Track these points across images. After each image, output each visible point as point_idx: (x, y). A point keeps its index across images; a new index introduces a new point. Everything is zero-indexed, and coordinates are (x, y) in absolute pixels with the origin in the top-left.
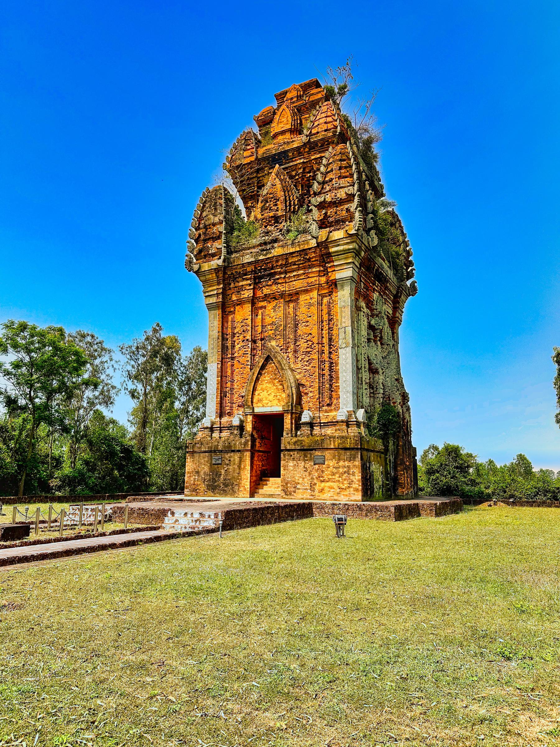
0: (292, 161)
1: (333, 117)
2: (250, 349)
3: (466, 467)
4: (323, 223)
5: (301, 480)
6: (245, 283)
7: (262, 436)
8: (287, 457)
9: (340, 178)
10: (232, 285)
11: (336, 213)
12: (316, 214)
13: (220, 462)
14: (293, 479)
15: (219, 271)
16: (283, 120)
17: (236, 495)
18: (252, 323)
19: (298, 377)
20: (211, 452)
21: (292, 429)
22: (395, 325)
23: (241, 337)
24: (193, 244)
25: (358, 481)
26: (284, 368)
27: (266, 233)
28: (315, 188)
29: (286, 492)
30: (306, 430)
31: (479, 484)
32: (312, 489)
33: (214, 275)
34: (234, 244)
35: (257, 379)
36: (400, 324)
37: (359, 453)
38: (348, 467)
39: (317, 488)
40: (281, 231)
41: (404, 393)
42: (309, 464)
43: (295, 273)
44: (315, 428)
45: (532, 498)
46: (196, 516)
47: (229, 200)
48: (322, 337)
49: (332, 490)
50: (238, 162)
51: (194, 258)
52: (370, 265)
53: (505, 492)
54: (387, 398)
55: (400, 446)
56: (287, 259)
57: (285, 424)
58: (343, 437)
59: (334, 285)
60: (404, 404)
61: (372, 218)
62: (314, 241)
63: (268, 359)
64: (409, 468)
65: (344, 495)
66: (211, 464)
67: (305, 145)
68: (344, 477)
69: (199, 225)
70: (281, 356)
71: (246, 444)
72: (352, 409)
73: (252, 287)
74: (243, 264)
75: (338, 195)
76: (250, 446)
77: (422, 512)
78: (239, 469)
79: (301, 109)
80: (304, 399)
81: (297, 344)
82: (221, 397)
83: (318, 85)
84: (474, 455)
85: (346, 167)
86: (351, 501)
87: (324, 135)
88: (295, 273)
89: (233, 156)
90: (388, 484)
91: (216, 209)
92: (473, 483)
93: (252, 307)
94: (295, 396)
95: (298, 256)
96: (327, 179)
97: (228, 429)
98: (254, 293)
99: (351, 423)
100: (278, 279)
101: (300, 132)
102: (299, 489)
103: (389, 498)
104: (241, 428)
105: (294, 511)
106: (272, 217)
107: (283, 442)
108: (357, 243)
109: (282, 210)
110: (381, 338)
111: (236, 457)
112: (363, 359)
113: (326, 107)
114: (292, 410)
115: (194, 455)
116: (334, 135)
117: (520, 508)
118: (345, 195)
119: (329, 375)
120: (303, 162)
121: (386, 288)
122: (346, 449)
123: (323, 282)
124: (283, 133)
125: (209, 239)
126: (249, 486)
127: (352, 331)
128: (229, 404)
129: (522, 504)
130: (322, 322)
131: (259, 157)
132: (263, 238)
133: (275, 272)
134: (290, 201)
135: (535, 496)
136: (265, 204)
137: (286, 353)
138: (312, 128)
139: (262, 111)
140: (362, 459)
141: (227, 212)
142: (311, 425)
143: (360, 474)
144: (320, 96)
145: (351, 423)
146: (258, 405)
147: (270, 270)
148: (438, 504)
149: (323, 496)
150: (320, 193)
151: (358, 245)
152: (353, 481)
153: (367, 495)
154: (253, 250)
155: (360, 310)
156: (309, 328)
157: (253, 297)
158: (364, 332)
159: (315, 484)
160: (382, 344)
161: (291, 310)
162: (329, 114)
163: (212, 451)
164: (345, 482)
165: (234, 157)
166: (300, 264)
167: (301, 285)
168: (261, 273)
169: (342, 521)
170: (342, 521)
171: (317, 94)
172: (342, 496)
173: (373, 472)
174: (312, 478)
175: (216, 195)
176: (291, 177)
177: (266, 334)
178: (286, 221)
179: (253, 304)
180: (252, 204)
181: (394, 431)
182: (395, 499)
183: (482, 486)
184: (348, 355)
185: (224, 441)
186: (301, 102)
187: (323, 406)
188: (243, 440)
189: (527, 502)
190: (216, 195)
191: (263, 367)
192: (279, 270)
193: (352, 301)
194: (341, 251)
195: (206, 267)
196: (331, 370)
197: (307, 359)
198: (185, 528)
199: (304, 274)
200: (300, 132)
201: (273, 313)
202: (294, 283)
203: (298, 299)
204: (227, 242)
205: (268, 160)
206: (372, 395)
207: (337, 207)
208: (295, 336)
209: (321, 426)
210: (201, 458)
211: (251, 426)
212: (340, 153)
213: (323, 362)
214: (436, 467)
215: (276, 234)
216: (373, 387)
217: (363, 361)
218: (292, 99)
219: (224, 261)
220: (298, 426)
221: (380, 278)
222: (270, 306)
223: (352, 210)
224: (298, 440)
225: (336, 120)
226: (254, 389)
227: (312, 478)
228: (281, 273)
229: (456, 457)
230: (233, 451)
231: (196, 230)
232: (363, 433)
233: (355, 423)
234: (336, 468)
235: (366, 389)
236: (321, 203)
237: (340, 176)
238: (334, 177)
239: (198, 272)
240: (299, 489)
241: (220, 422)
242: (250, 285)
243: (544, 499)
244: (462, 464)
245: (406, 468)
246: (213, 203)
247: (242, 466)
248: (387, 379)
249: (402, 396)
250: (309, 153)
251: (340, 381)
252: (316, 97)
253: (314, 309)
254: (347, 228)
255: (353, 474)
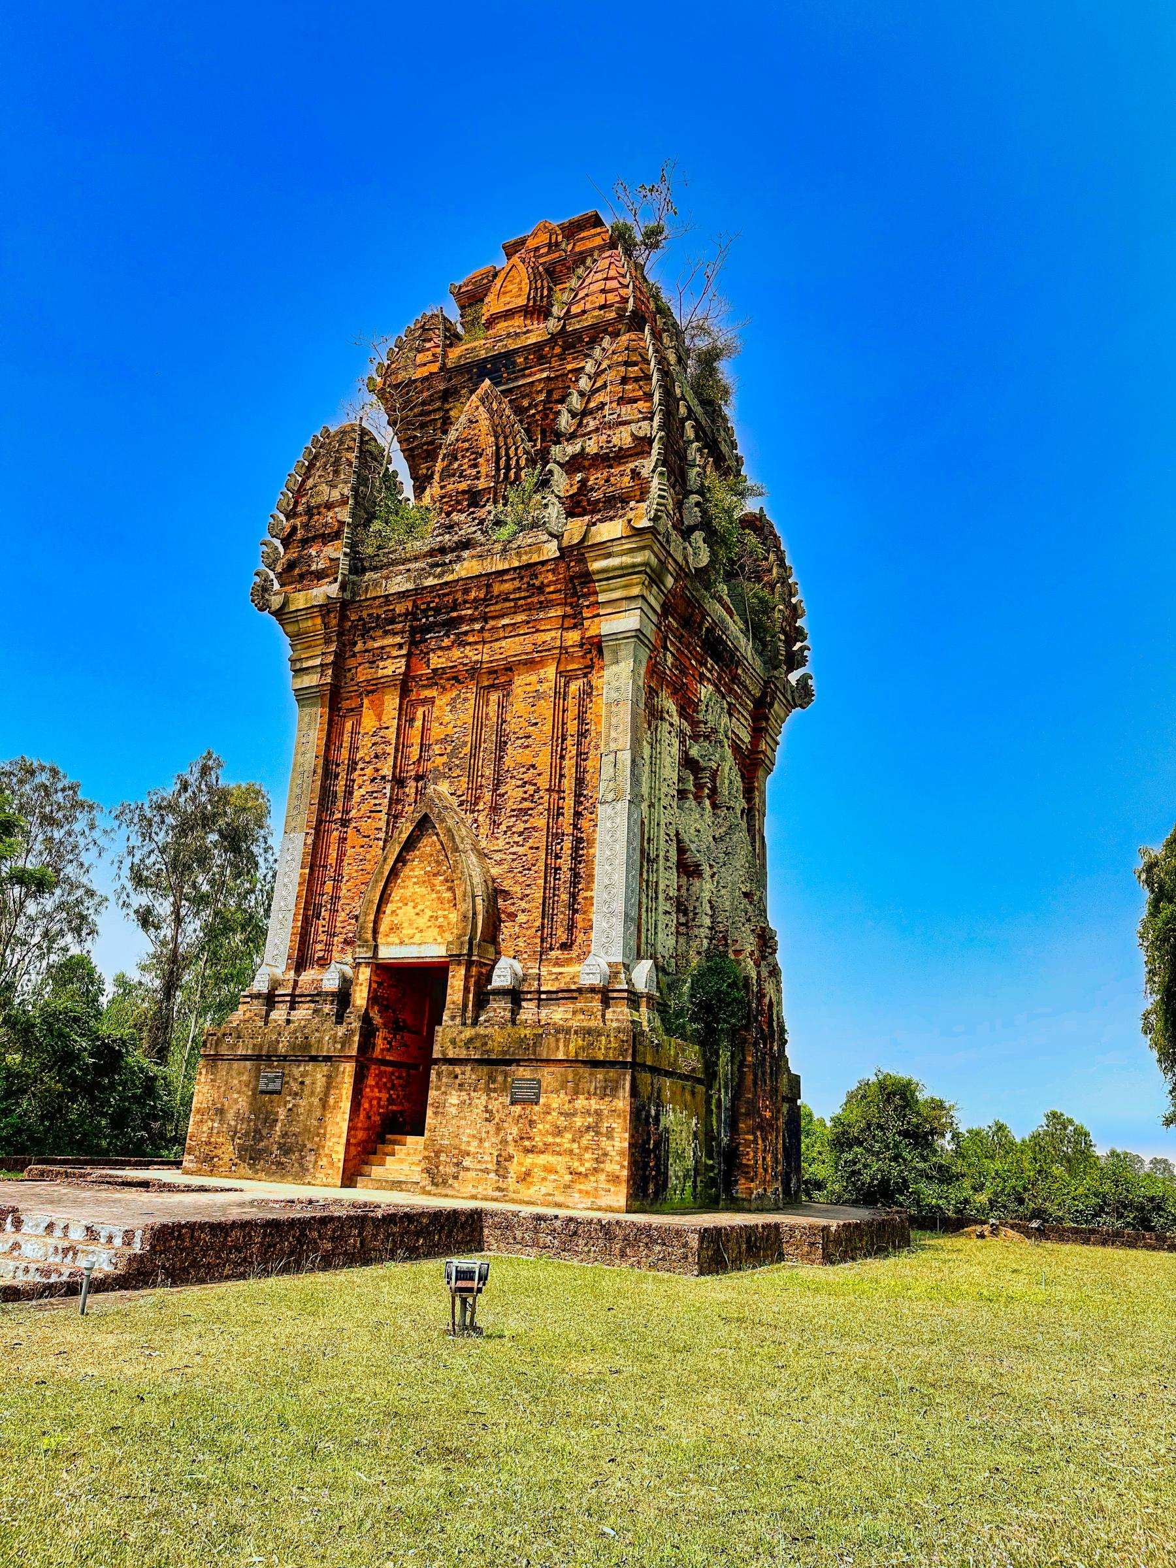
0: (524, 376)
1: (621, 279)
2: (386, 800)
3: (927, 1133)
4: (578, 504)
5: (475, 1143)
6: (390, 640)
7: (396, 1022)
8: (444, 1080)
9: (621, 401)
10: (359, 647)
11: (607, 481)
12: (562, 483)
13: (276, 1086)
14: (457, 1141)
15: (329, 612)
16: (509, 288)
17: (309, 1179)
18: (398, 737)
19: (494, 871)
20: (258, 1058)
21: (465, 1005)
22: (756, 770)
23: (369, 771)
24: (276, 548)
25: (621, 1153)
26: (461, 847)
27: (447, 528)
28: (563, 423)
29: (436, 1179)
30: (499, 1009)
31: (958, 1179)
32: (501, 1172)
33: (319, 621)
34: (370, 551)
35: (394, 873)
36: (769, 771)
37: (628, 1078)
38: (598, 1113)
39: (514, 1168)
40: (481, 522)
41: (763, 929)
42: (500, 1101)
43: (506, 621)
44: (524, 1004)
45: (1086, 1222)
46: (77, 1235)
47: (369, 454)
48: (562, 776)
49: (553, 1177)
50: (402, 376)
51: (275, 582)
52: (692, 615)
53: (1021, 1201)
54: (720, 939)
55: (747, 1066)
56: (489, 586)
57: (449, 991)
58: (589, 1032)
59: (595, 648)
60: (764, 958)
61: (698, 504)
62: (554, 544)
63: (424, 825)
64: (771, 1125)
65: (580, 1191)
66: (254, 1090)
67: (553, 338)
68: (584, 1142)
69: (295, 506)
70: (458, 822)
71: (346, 1040)
72: (620, 959)
73: (404, 652)
74: (387, 596)
75: (615, 440)
76: (356, 1046)
77: (788, 1249)
78: (324, 1108)
79: (554, 271)
80: (507, 929)
81: (501, 791)
82: (305, 916)
83: (597, 222)
84: (947, 1105)
85: (636, 380)
86: (599, 1209)
87: (596, 317)
88: (506, 621)
89: (393, 363)
90: (712, 1166)
91: (336, 472)
92: (945, 1175)
93: (402, 698)
94: (480, 919)
95: (514, 579)
96: (592, 405)
97: (313, 1002)
98: (408, 666)
99: (615, 995)
100: (466, 633)
101: (546, 314)
102: (468, 1169)
103: (710, 1205)
104: (343, 997)
105: (418, 1234)
106: (464, 492)
107: (438, 1038)
108: (653, 552)
109: (487, 476)
110: (714, 791)
111: (319, 1076)
112: (663, 837)
113: (607, 261)
114: (470, 954)
115: (216, 1066)
116: (620, 317)
117: (1056, 1246)
118: (630, 439)
119: (571, 869)
120: (548, 378)
121: (735, 678)
122: (595, 1064)
123: (570, 643)
124: (508, 314)
125: (315, 537)
126: (342, 1156)
127: (633, 761)
128: (323, 937)
129: (1062, 1236)
130: (564, 740)
131: (450, 365)
132: (438, 539)
133: (460, 617)
134: (509, 459)
135: (1095, 1216)
136: (451, 464)
137: (473, 812)
138: (571, 304)
139: (471, 275)
140: (634, 1092)
141: (362, 480)
142: (515, 996)
143: (627, 1135)
144: (598, 241)
145: (615, 995)
146: (389, 939)
147: (447, 613)
148: (833, 1229)
149: (530, 1192)
150: (572, 437)
151: (656, 556)
152: (606, 1155)
153: (646, 1195)
154: (412, 566)
155: (662, 719)
156: (531, 754)
157: (404, 674)
158: (670, 771)
159: (510, 1158)
160: (714, 806)
161: (492, 709)
162: (612, 273)
163: (263, 1058)
164: (587, 1156)
165: (393, 366)
166: (520, 599)
167: (519, 649)
168: (427, 617)
169: (472, 1279)
170: (472, 1279)
171: (592, 239)
172: (577, 1195)
173: (667, 1130)
174: (504, 1142)
175: (341, 443)
176: (519, 411)
177: (430, 765)
178: (495, 502)
179: (405, 692)
180: (428, 469)
181: (734, 1025)
182: (727, 1209)
183: (967, 1183)
184: (618, 820)
185: (295, 1031)
186: (557, 255)
187: (551, 949)
188: (341, 1031)
189: (1076, 1231)
190: (341, 443)
191: (410, 844)
192: (470, 612)
193: (636, 689)
194: (615, 569)
195: (300, 601)
196: (576, 857)
197: (520, 827)
198: (26, 1270)
199: (528, 622)
200: (546, 314)
201: (450, 715)
202: (503, 643)
203: (510, 682)
204: (353, 545)
205: (469, 371)
206: (683, 929)
207: (611, 467)
208: (497, 772)
209: (540, 1000)
210: (234, 1073)
211: (365, 995)
212: (627, 349)
213: (559, 836)
214: (855, 1131)
215: (469, 530)
216: (686, 909)
217: (662, 842)
218: (537, 249)
219: (343, 588)
220: (482, 996)
221: (717, 648)
222: (442, 701)
223: (645, 473)
224: (478, 1035)
225: (627, 286)
226: (384, 899)
227: (504, 1142)
228: (473, 620)
229: (904, 1107)
230: (314, 1059)
231: (288, 518)
232: (645, 1024)
233: (625, 995)
234: (566, 1115)
235: (666, 912)
236: (573, 457)
237: (621, 398)
238: (608, 399)
239: (280, 614)
240: (468, 1169)
241: (296, 982)
242: (400, 646)
243: (1118, 1224)
244: (917, 1126)
245: (764, 1127)
246: (332, 460)
247: (331, 1101)
248: (723, 892)
249: (759, 936)
250: (562, 357)
251: (595, 886)
252: (590, 245)
253: (546, 708)
254: (631, 515)
255: (610, 1135)
